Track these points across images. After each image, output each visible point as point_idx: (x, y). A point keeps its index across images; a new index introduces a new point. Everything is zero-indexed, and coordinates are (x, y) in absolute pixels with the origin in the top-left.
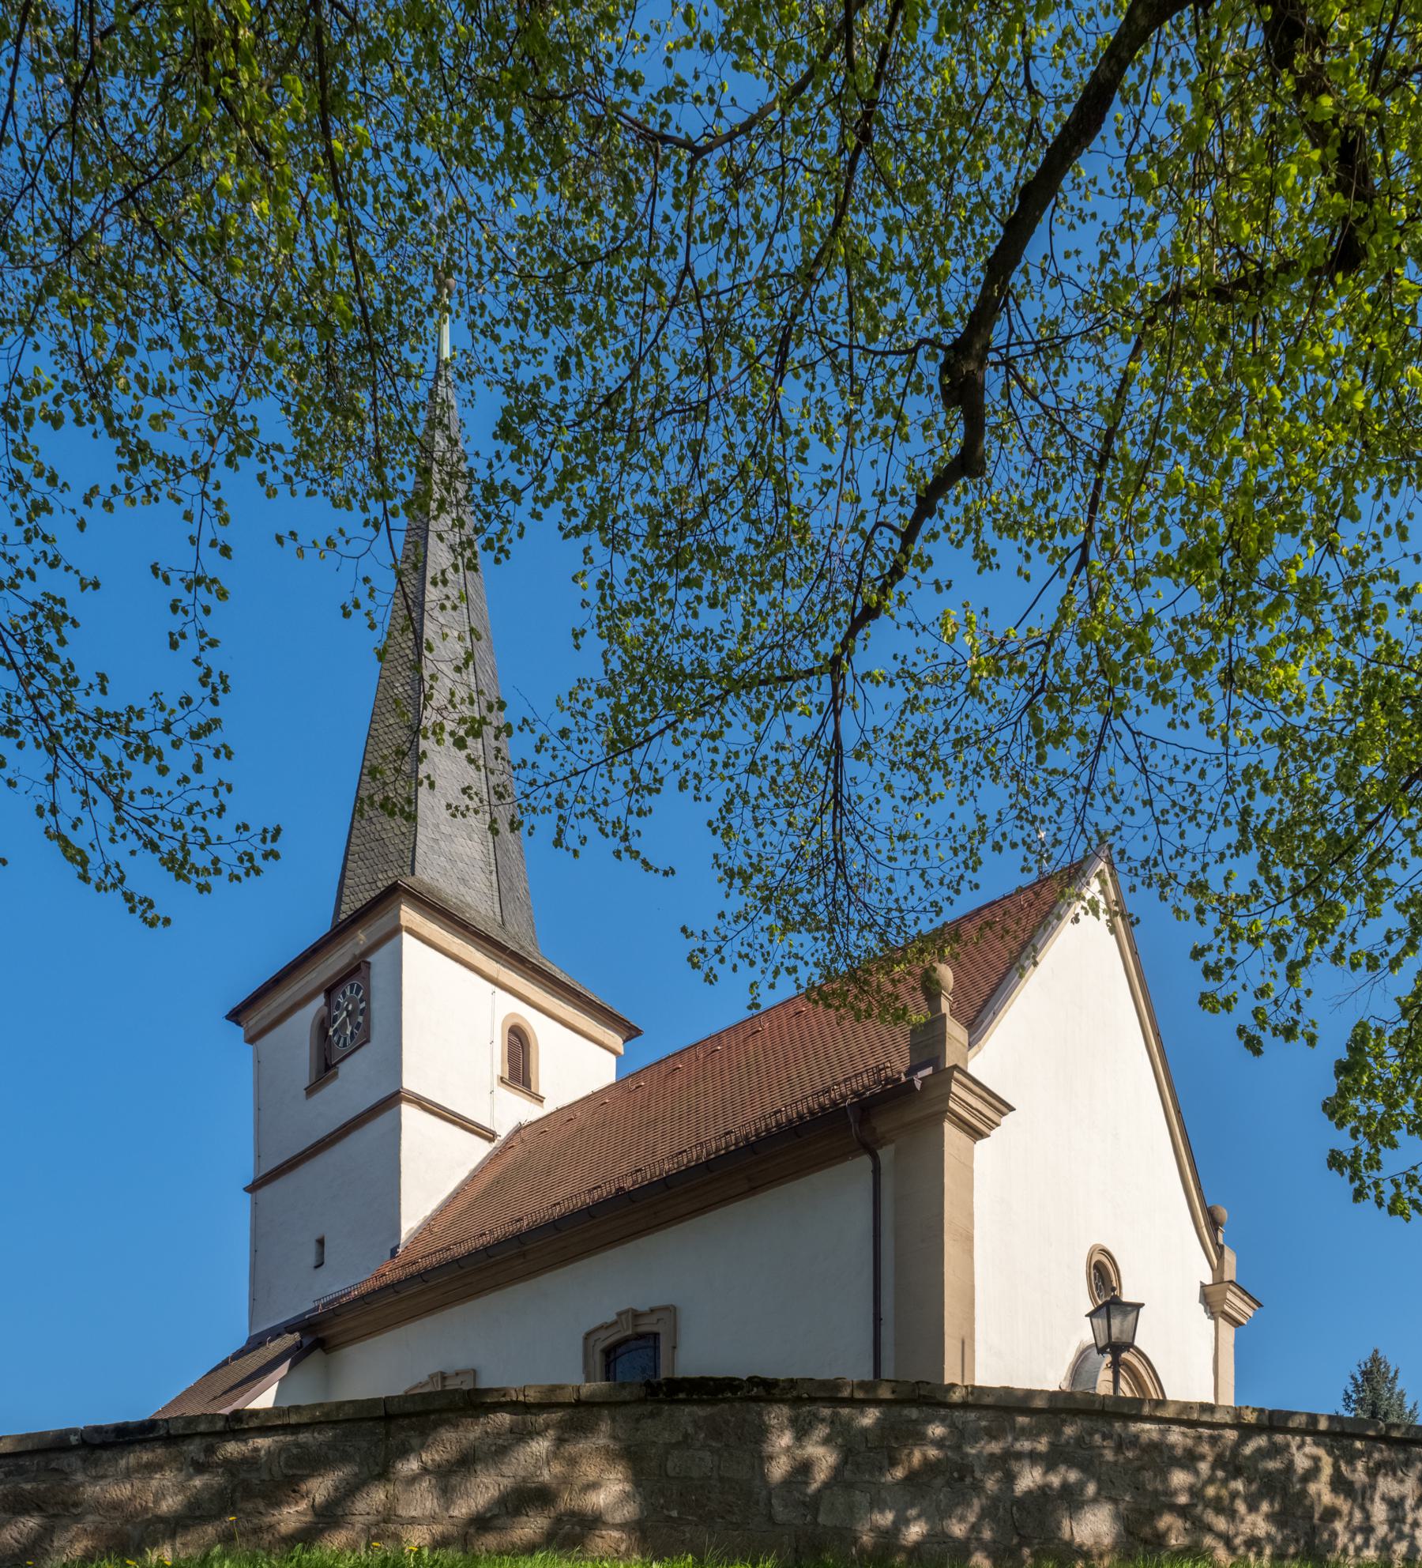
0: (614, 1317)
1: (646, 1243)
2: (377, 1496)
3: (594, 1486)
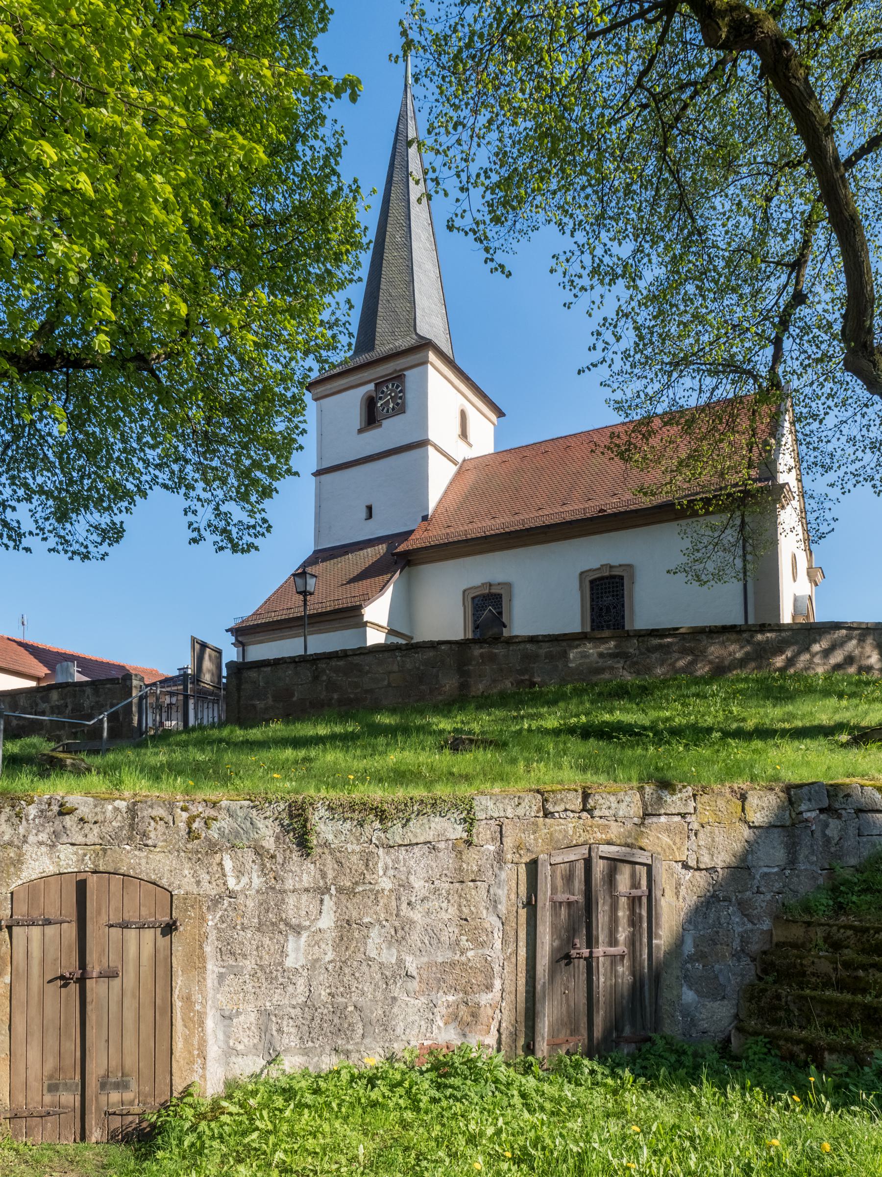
0: (598, 566)
1: (612, 534)
2: (805, 657)
3: (869, 657)
